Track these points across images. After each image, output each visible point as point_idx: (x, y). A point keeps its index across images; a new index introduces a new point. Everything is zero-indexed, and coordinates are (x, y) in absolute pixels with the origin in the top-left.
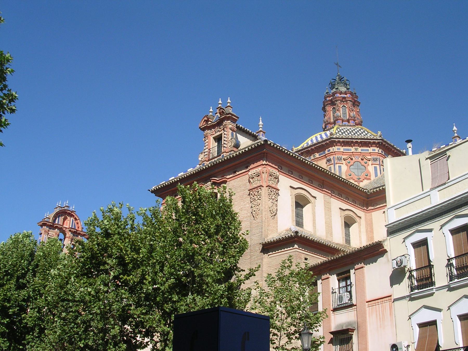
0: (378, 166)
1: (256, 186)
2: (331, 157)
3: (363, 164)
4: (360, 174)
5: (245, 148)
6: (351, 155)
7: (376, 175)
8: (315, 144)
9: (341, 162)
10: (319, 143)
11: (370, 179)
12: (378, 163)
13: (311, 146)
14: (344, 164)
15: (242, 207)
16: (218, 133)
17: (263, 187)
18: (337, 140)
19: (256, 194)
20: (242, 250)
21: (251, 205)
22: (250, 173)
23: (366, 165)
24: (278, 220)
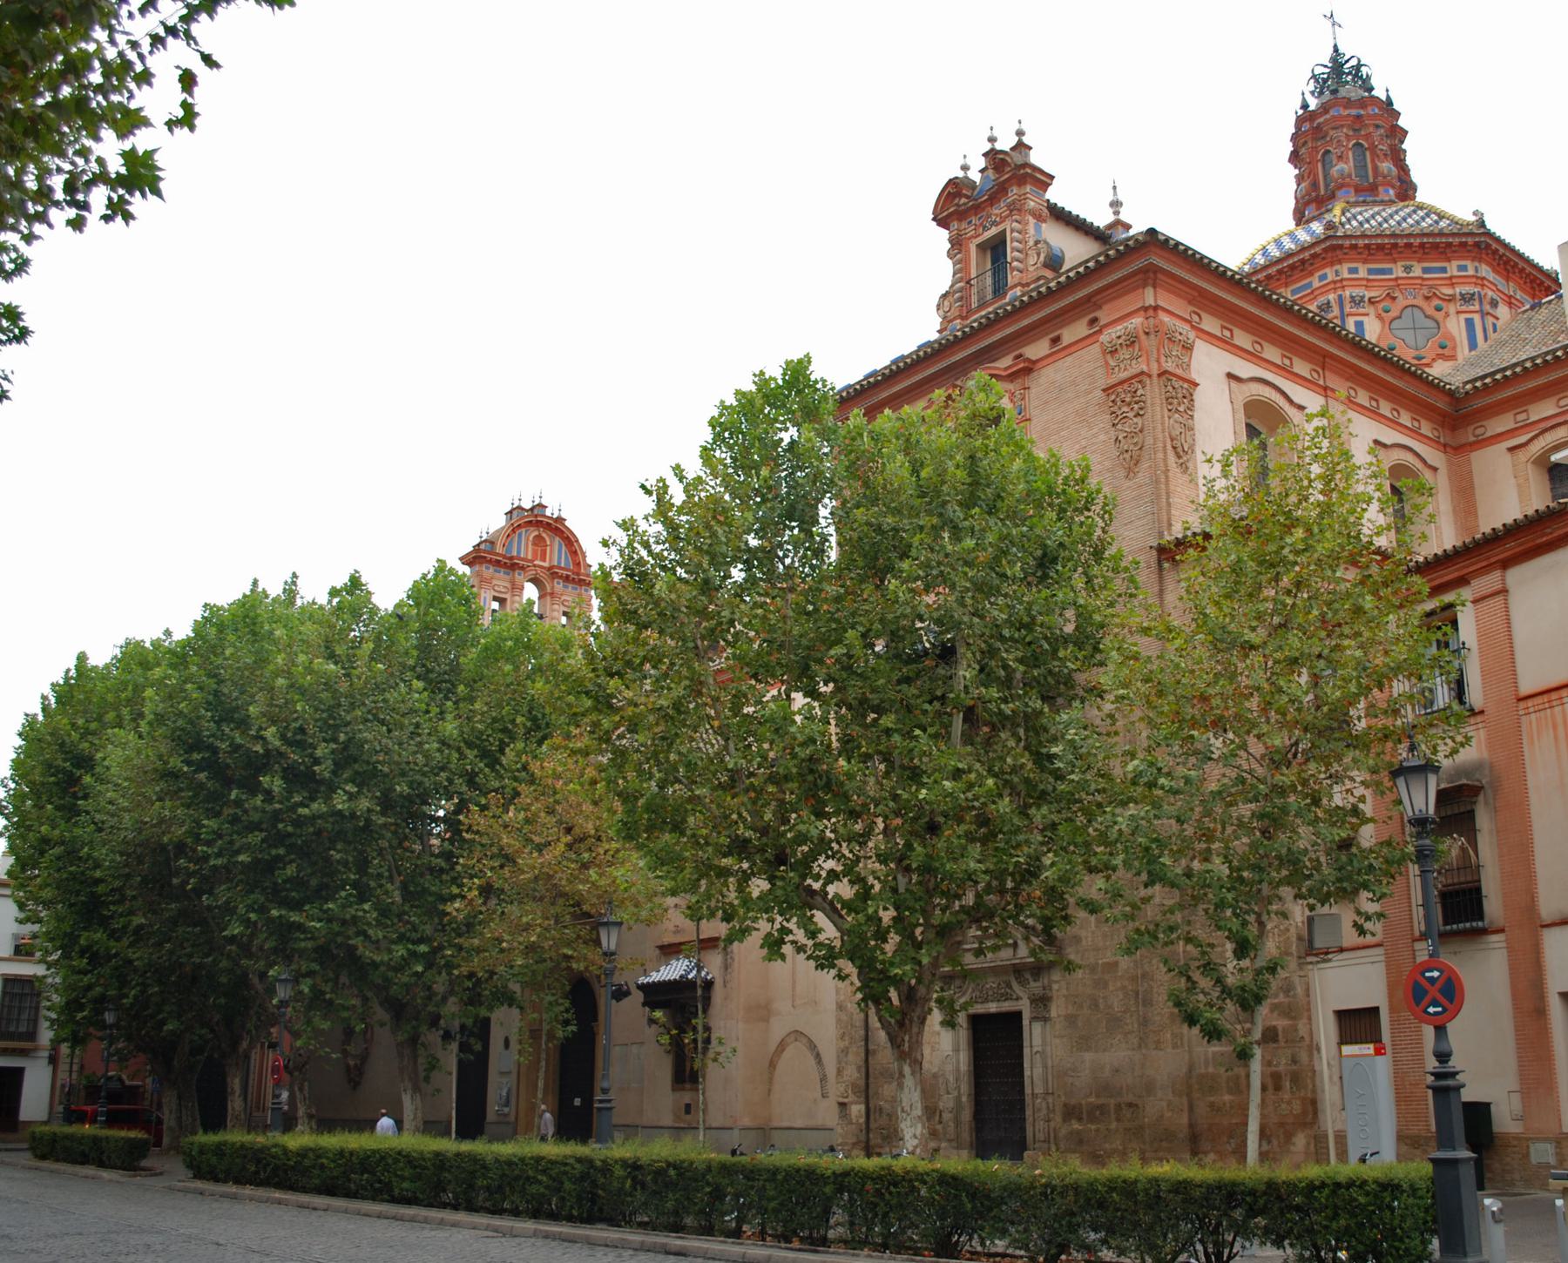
0: (1477, 318)
1: (1124, 375)
2: (1331, 297)
3: (1430, 311)
4: (1421, 343)
5: (1087, 261)
7: (1473, 345)
8: (1280, 261)
9: (1361, 310)
10: (1290, 255)
11: (1453, 358)
12: (1477, 307)
13: (1265, 267)
14: (1372, 315)
15: (1084, 443)
16: (994, 231)
17: (1150, 376)
18: (1347, 243)
21: (1113, 434)
22: (1104, 338)
23: (1439, 316)
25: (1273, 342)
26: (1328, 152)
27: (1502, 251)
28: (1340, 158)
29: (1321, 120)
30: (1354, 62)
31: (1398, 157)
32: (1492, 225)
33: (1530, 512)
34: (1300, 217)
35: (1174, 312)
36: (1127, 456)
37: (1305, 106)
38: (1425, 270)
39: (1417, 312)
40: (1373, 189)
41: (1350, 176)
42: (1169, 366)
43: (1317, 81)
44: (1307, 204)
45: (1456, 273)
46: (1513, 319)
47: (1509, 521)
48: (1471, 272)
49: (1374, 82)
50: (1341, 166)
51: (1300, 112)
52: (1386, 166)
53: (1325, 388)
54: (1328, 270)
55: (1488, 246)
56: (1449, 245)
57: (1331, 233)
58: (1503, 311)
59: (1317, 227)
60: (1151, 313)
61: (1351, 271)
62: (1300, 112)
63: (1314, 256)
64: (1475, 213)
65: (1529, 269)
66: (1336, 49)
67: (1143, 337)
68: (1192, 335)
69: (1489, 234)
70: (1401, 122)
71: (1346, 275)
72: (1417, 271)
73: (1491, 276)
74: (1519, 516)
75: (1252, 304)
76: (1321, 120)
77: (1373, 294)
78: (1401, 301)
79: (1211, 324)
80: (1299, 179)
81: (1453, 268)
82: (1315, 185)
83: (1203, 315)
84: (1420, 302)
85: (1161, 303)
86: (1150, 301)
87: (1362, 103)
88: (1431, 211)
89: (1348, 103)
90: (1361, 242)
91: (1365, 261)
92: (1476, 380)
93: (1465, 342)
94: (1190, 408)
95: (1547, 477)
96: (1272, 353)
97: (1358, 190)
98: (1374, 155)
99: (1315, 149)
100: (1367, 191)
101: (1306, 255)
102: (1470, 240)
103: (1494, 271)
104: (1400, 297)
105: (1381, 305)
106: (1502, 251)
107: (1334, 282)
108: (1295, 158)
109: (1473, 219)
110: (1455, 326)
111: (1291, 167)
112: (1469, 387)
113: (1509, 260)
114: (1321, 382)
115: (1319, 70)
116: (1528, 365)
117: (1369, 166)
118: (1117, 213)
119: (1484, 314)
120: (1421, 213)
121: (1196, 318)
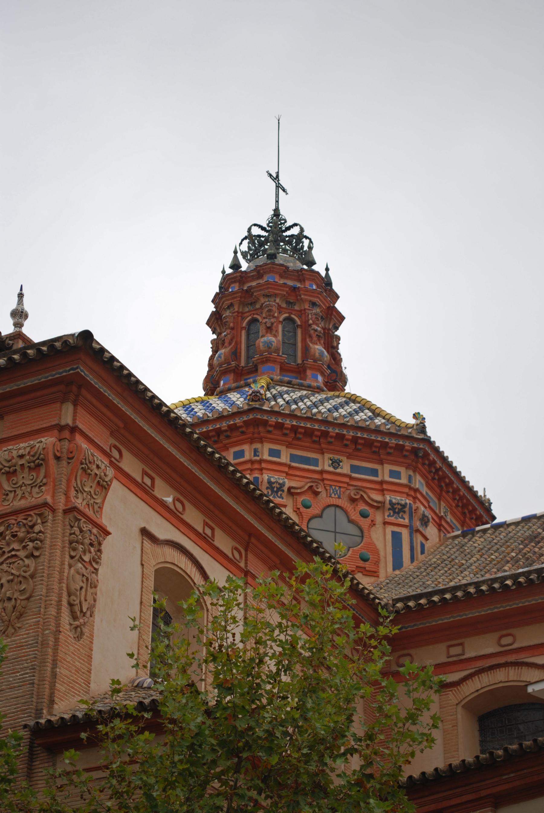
0: (405, 533)
1: (23, 503)
3: (355, 516)
6: (313, 480)
7: (398, 564)
12: (406, 521)
17: (53, 510)
18: (273, 420)
19: (21, 535)
20: (422, 524)
23: (364, 523)
24: (95, 647)
25: (197, 505)
26: (254, 321)
27: (439, 464)
28: (269, 329)
29: (254, 284)
30: (295, 231)
31: (332, 343)
32: (433, 432)
33: (456, 762)
34: (211, 385)
35: (93, 439)
36: (9, 605)
37: (235, 266)
38: (354, 469)
39: (340, 514)
40: (300, 371)
41: (277, 351)
42: (79, 502)
43: (252, 242)
44: (224, 373)
45: (387, 478)
46: (442, 542)
47: (429, 769)
48: (404, 480)
49: (316, 254)
50: (270, 338)
51: (229, 271)
52: (318, 348)
53: (247, 573)
54: (246, 447)
55: (426, 455)
56: (385, 445)
57: (256, 405)
58: (431, 531)
59: (238, 399)
60: (66, 434)
61: (272, 453)
62: (229, 271)
63: (233, 428)
64: (416, 416)
65: (463, 491)
66: (277, 213)
67: (52, 461)
68: (111, 472)
69: (428, 442)
70: (339, 305)
71: (266, 457)
72: (345, 468)
73: (424, 490)
74: (441, 765)
75: (184, 453)
76: (254, 284)
77: (293, 484)
78: (324, 498)
79: (131, 465)
80: (216, 346)
81: (385, 472)
82: (235, 354)
83: (125, 452)
84: (344, 502)
85: (81, 426)
86: (67, 419)
87: (300, 276)
88: (364, 405)
89: (285, 272)
90: (288, 422)
91: (289, 445)
92: (409, 598)
93: (390, 558)
94: (96, 560)
95: (476, 727)
96: (194, 517)
97: (284, 369)
98: (306, 334)
99: (241, 315)
100: (295, 372)
101: (224, 425)
102: (408, 444)
103: (428, 485)
104: (323, 494)
105: (301, 499)
106: (439, 464)
107: (252, 462)
108: (215, 321)
109: (412, 421)
110: (381, 538)
111: (209, 330)
112: (399, 605)
113: (445, 476)
114: (242, 565)
115: (256, 231)
116: (472, 590)
117: (299, 345)
118: (18, 325)
119: (413, 531)
120: (355, 406)
121: (115, 454)
